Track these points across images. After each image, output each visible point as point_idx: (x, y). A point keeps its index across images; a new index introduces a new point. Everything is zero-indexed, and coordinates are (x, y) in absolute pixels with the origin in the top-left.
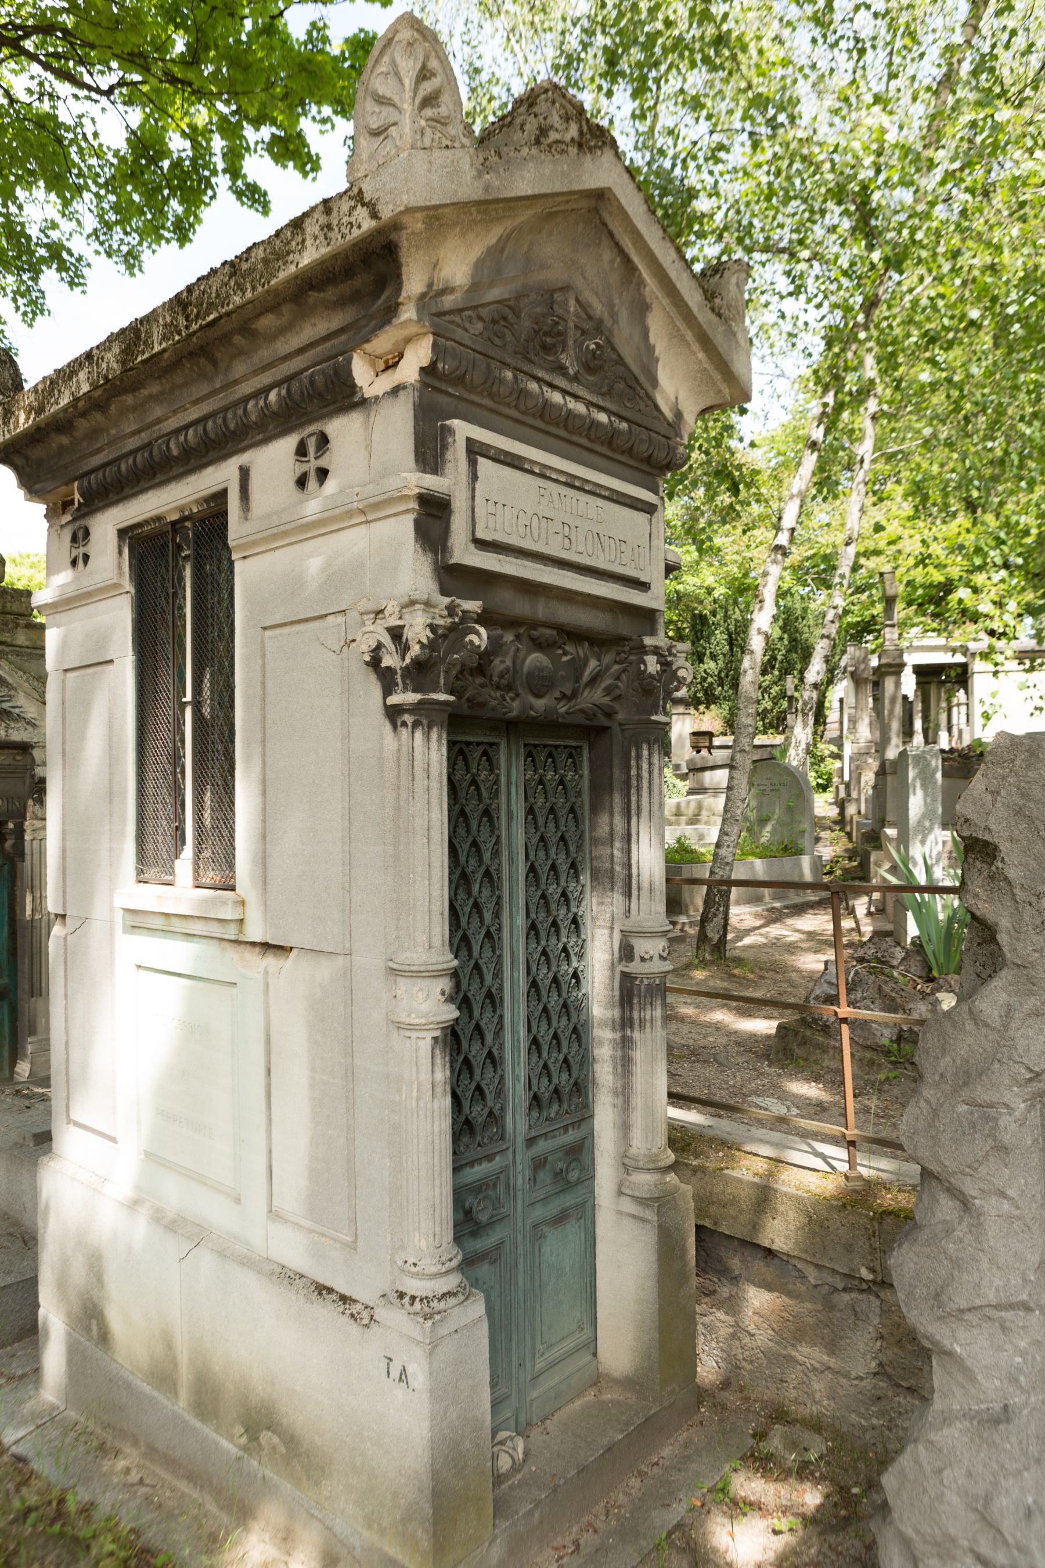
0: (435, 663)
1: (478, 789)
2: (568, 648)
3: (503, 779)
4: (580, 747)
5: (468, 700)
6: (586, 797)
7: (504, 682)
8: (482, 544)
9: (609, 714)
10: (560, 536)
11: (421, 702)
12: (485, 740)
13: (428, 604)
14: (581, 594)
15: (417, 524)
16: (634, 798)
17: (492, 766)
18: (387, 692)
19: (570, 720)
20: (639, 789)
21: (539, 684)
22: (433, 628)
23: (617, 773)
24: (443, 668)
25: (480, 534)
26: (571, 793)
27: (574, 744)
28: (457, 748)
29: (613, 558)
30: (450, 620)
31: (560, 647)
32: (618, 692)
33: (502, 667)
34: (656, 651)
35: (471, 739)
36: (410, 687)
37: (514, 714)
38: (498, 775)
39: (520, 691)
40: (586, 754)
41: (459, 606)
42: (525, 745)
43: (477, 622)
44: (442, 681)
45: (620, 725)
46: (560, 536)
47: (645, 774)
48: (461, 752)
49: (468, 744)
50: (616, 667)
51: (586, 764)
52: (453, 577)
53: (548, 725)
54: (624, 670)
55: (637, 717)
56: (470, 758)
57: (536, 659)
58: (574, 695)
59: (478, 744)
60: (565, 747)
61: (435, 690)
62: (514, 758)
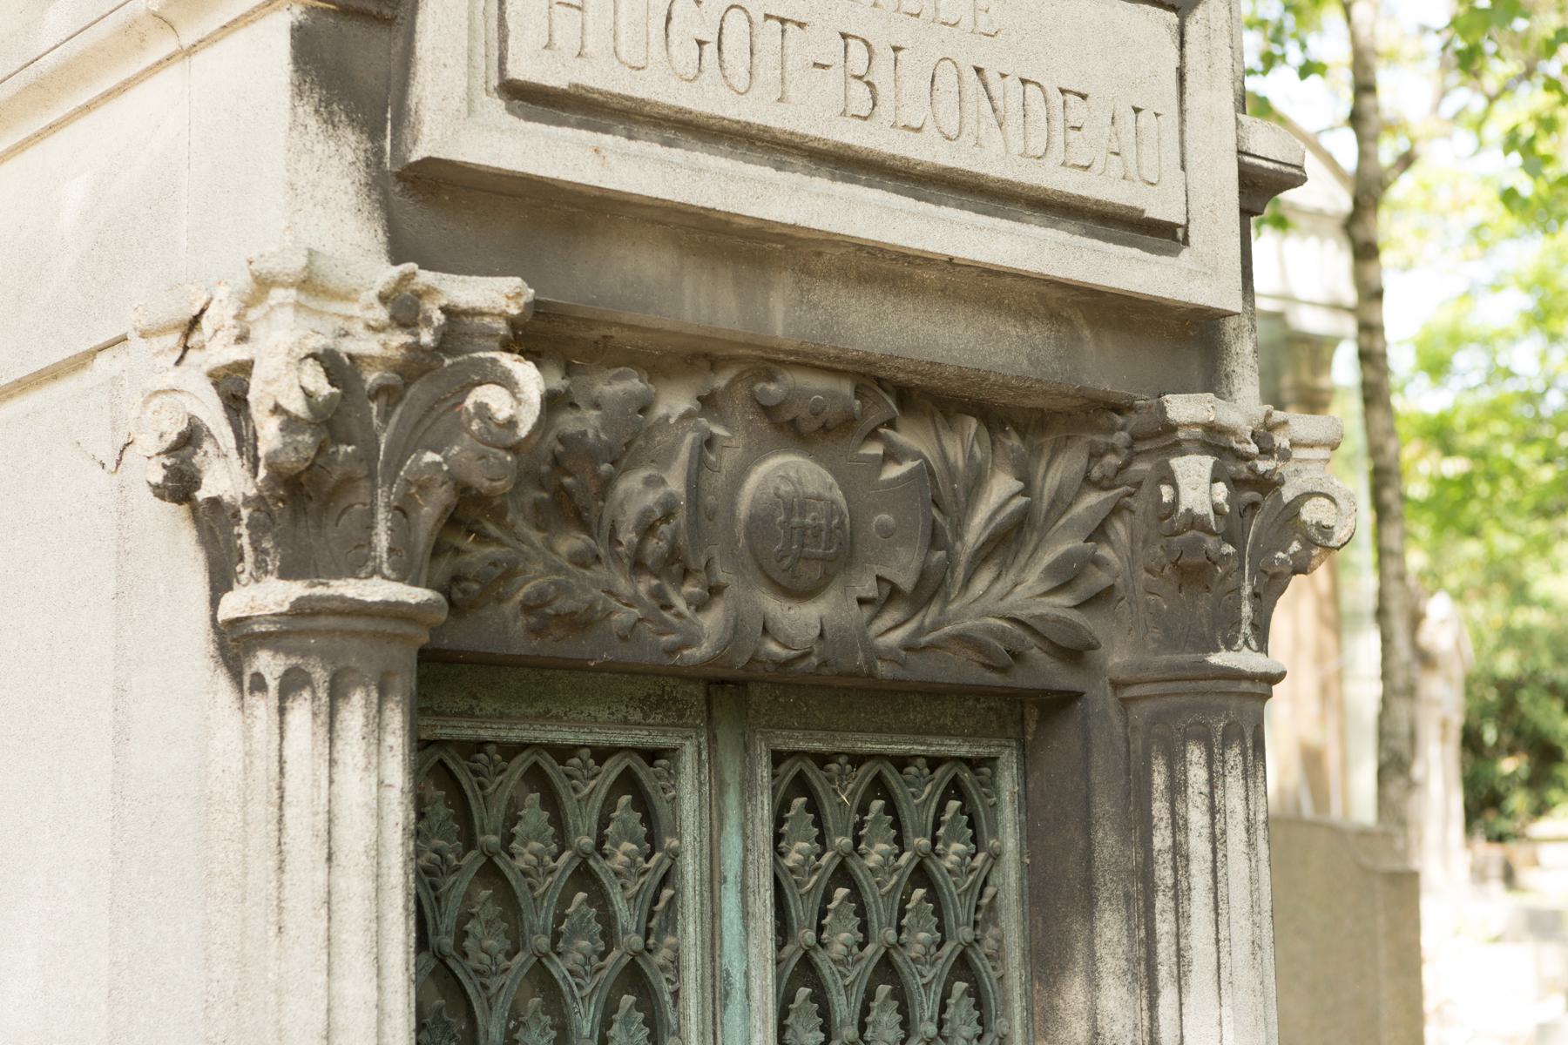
0: (348, 482)
1: (600, 898)
2: (902, 438)
3: (691, 868)
4: (991, 761)
5: (527, 608)
6: (1011, 928)
7: (656, 546)
8: (527, 99)
9: (1075, 653)
10: (834, 77)
11: (302, 610)
12: (622, 739)
13: (311, 285)
14: (925, 260)
15: (305, 45)
16: (1164, 926)
17: (653, 828)
18: (221, 581)
19: (924, 669)
20: (1179, 894)
21: (803, 554)
22: (333, 364)
23: (1107, 843)
24: (383, 498)
25: (523, 69)
26: (959, 912)
27: (964, 750)
28: (789, 770)
29: (1037, 144)
30: (400, 338)
31: (873, 435)
32: (1102, 579)
33: (652, 498)
34: (1214, 440)
35: (565, 736)
36: (273, 563)
37: (700, 652)
38: (675, 855)
39: (722, 575)
40: (1008, 782)
41: (430, 291)
42: (778, 758)
43: (507, 348)
44: (382, 540)
45: (1117, 685)
46: (834, 77)
47: (1198, 846)
48: (801, 785)
49: (563, 753)
50: (1092, 499)
51: (1009, 817)
52: (432, 205)
53: (833, 688)
54: (1117, 510)
55: (1164, 658)
56: (569, 802)
57: (782, 473)
58: (929, 589)
59: (601, 754)
60: (934, 762)
61: (358, 564)
62: (732, 799)
